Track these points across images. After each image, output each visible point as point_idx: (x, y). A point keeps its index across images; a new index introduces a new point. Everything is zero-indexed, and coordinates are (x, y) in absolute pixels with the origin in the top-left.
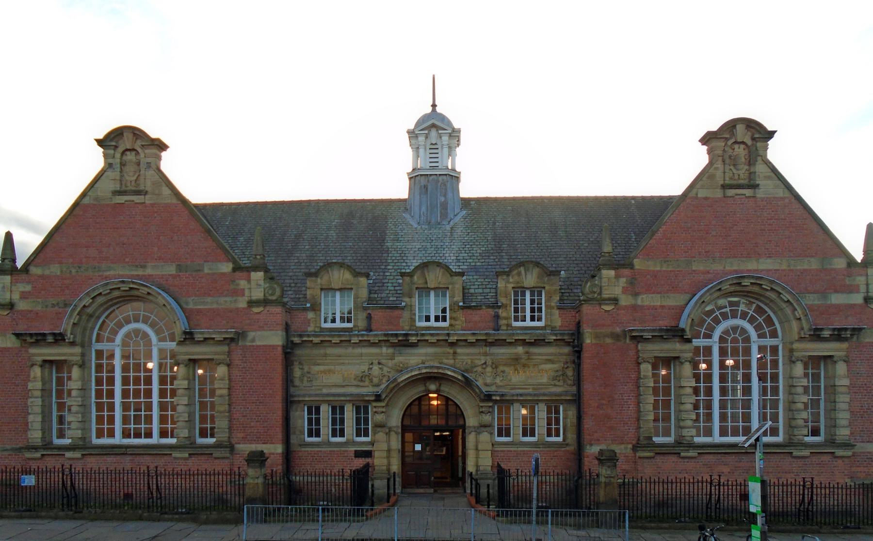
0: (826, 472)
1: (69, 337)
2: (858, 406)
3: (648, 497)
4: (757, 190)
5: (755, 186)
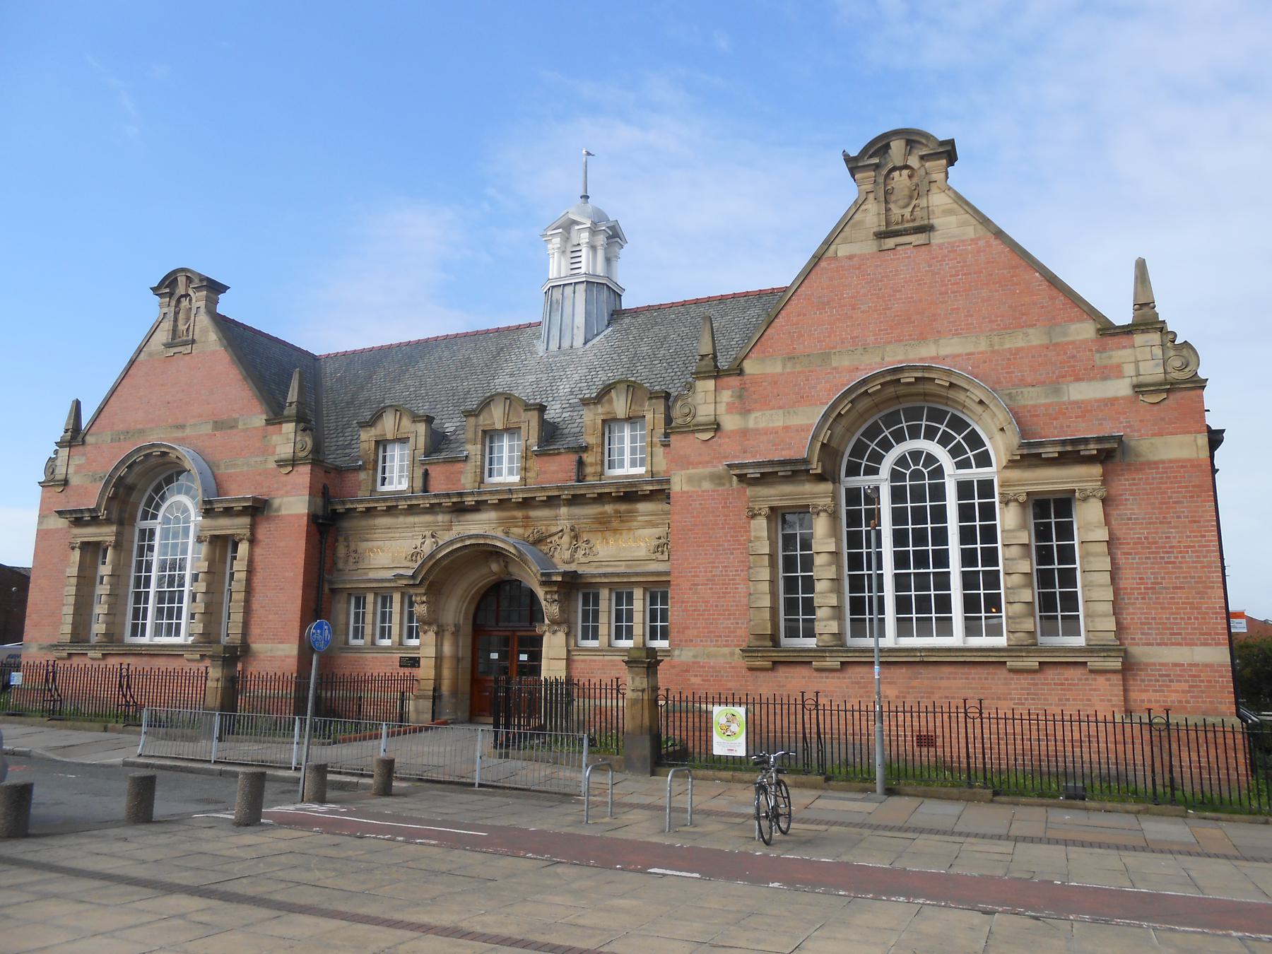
1: (102, 514)
2: (1133, 578)
4: (931, 234)
5: (927, 229)
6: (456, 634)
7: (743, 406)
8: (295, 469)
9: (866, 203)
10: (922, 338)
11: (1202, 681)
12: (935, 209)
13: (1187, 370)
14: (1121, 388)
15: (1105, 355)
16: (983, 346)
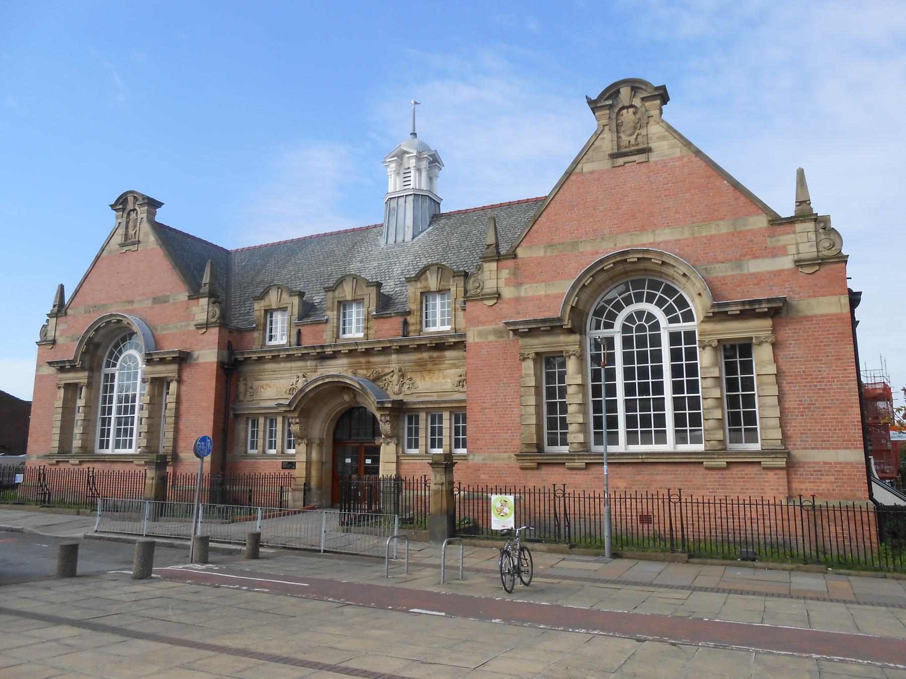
0: (752, 489)
1: (78, 364)
3: (532, 515)
4: (650, 154)
5: (647, 150)
6: (321, 445)
7: (516, 280)
8: (209, 330)
9: (603, 133)
10: (643, 230)
11: (844, 475)
12: (652, 136)
13: (833, 249)
14: (786, 263)
15: (774, 239)
16: (687, 234)
